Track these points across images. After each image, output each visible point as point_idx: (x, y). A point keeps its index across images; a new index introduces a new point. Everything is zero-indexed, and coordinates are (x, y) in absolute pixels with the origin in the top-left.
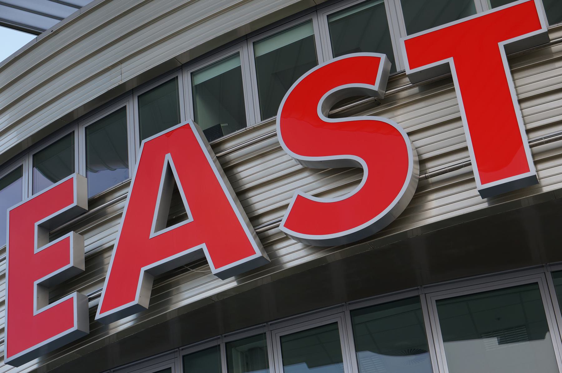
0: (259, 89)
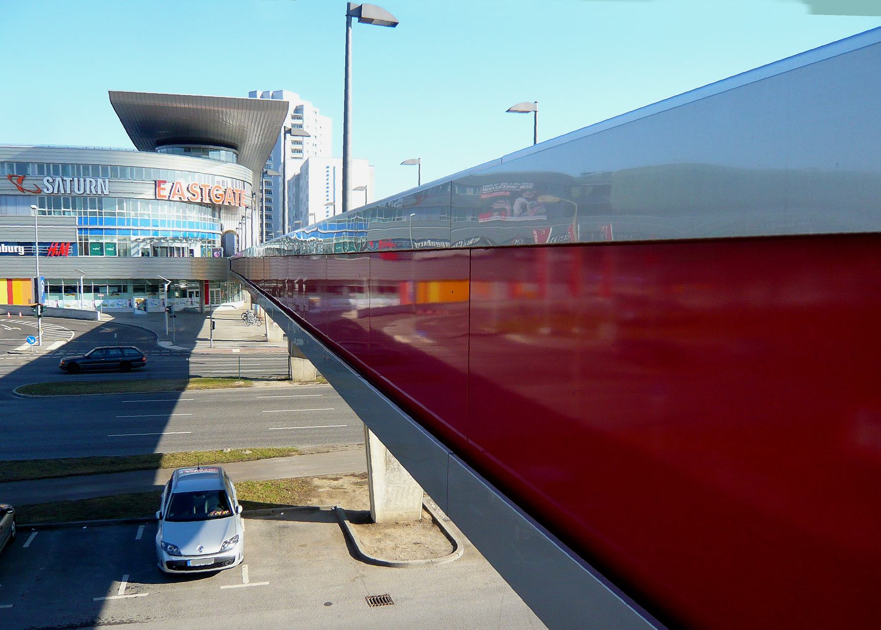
0: (805, 56)
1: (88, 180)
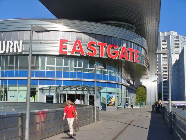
1: (8, 42)
